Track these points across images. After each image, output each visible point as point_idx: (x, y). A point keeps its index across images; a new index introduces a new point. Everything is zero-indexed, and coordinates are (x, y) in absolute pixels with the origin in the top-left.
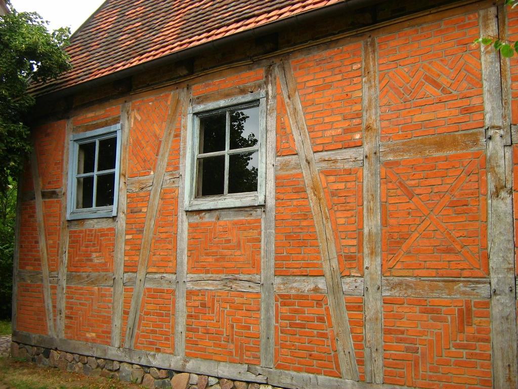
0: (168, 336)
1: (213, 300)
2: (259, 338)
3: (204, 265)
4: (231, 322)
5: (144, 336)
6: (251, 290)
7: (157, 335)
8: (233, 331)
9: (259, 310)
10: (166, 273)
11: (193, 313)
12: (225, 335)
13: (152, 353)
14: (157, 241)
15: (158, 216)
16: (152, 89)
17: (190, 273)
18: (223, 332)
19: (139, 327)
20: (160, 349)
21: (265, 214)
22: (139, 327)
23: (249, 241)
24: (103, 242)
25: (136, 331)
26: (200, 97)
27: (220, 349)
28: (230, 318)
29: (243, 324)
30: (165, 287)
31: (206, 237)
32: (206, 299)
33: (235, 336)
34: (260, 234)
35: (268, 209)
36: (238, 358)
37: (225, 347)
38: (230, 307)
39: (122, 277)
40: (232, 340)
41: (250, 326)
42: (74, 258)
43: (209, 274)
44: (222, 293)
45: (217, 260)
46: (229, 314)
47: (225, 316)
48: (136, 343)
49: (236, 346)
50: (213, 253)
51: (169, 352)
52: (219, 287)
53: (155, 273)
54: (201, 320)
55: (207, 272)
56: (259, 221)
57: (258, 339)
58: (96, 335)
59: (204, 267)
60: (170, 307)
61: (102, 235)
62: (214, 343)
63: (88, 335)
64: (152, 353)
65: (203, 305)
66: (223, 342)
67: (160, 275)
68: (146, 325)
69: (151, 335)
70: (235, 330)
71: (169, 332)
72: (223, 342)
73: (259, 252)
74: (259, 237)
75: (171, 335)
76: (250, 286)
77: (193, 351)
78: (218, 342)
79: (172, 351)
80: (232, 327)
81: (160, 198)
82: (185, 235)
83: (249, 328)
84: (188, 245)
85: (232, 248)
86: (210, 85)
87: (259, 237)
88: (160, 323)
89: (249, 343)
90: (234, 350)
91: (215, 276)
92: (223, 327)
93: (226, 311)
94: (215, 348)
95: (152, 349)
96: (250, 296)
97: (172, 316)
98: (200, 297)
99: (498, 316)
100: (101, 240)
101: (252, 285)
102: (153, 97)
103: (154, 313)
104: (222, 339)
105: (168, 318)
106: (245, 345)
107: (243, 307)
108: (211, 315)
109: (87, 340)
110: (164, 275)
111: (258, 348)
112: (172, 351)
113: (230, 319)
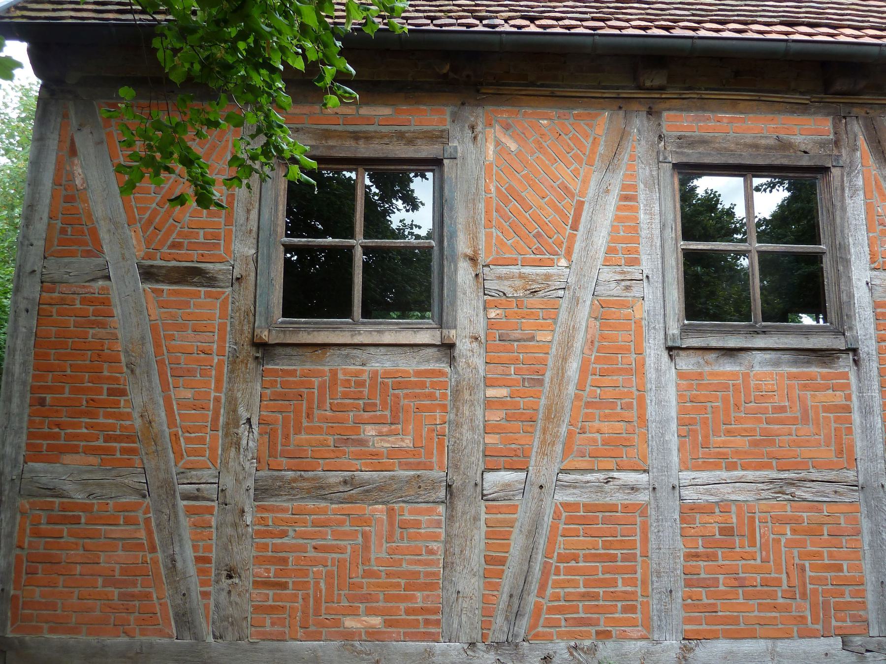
0: (634, 603)
1: (752, 520)
2: (863, 584)
3: (724, 454)
4: (797, 561)
5: (559, 610)
6: (837, 498)
7: (601, 603)
8: (804, 577)
9: (858, 534)
10: (618, 470)
11: (701, 549)
12: (785, 586)
13: (587, 643)
14: (588, 405)
15: (587, 351)
16: (547, 93)
17: (687, 469)
18: (780, 579)
19: (543, 587)
20: (610, 632)
21: (858, 370)
22: (543, 587)
23: (827, 409)
24: (404, 402)
25: (532, 599)
26: (685, 136)
27: (774, 614)
28: (795, 552)
29: (826, 562)
30: (619, 498)
31: (725, 400)
32: (734, 520)
33: (809, 586)
34: (848, 398)
35: (862, 354)
36: (819, 627)
37: (787, 608)
38: (794, 531)
39: (479, 481)
40: (804, 596)
41: (842, 565)
42: (287, 437)
43: (736, 469)
44: (773, 507)
45: (755, 444)
46: (790, 544)
47: (783, 549)
48: (534, 626)
49: (814, 607)
50: (745, 430)
51: (635, 635)
52: (764, 494)
53: (592, 471)
54: (721, 562)
55: (731, 467)
56: (845, 376)
57: (861, 587)
58: (385, 621)
59: (724, 457)
60: (635, 540)
61: (398, 386)
62: (759, 604)
63: (350, 623)
64: (587, 643)
65: (727, 531)
66: (781, 600)
67: (601, 476)
68: (557, 584)
69: (581, 604)
70: (809, 573)
71: (634, 593)
72: (781, 600)
73: (849, 431)
74: (848, 403)
75: (640, 599)
76: (836, 492)
77: (705, 627)
78: (769, 601)
79: (645, 632)
80: (803, 569)
81: (590, 316)
82: (160, 287)
83: (840, 568)
84: (678, 414)
85: (794, 421)
86: (709, 119)
87: (848, 403)
88: (608, 576)
89: (842, 595)
90: (808, 614)
91: (750, 475)
92: (779, 570)
93: (783, 541)
94: (762, 614)
95: (586, 636)
96: (835, 508)
97: (639, 559)
98: (718, 516)
99: (438, 333)
100: (397, 397)
101: (841, 488)
102: (553, 113)
103: (585, 556)
104: (780, 594)
105: (633, 563)
106: (833, 600)
107: (822, 530)
108: (748, 549)
109: (349, 636)
110: (616, 474)
111: (864, 602)
112: (645, 632)
113: (796, 554)
